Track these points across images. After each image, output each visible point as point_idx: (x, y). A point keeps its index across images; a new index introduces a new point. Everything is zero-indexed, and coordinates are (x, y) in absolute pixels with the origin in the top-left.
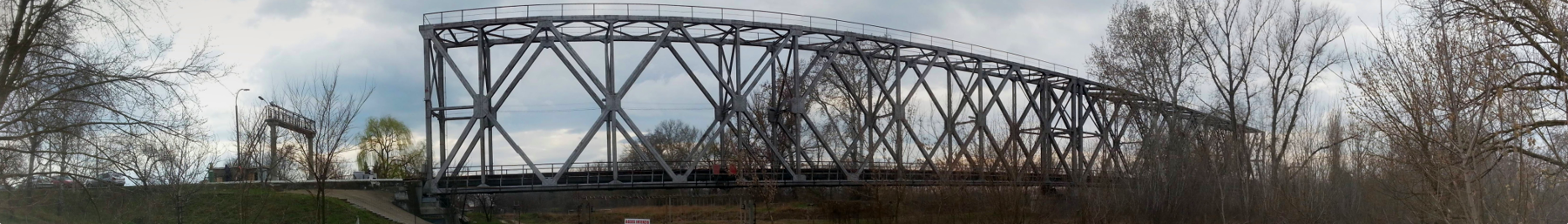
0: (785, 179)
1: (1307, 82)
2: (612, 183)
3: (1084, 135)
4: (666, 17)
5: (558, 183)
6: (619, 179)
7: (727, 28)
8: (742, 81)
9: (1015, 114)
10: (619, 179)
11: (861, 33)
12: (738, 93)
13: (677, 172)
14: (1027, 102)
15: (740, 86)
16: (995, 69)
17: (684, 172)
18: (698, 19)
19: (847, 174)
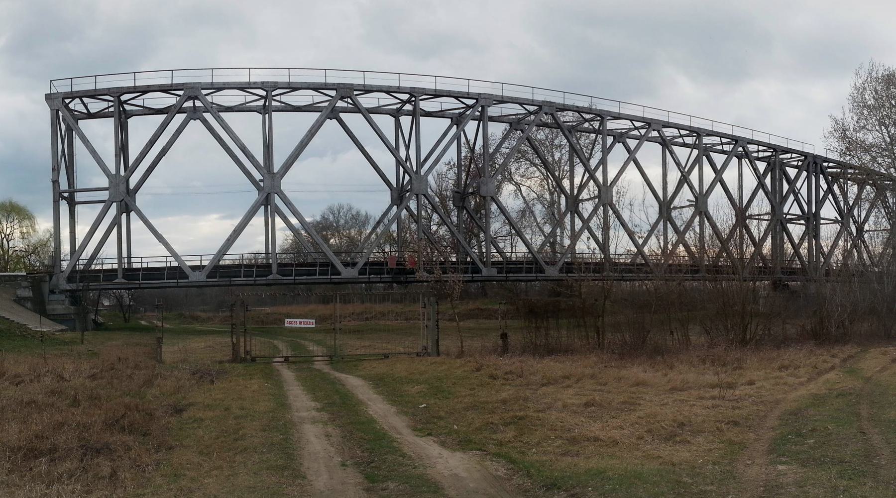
2: (270, 277)
5: (208, 277)
6: (278, 273)
10: (278, 273)
12: (417, 172)
15: (420, 165)
17: (354, 264)
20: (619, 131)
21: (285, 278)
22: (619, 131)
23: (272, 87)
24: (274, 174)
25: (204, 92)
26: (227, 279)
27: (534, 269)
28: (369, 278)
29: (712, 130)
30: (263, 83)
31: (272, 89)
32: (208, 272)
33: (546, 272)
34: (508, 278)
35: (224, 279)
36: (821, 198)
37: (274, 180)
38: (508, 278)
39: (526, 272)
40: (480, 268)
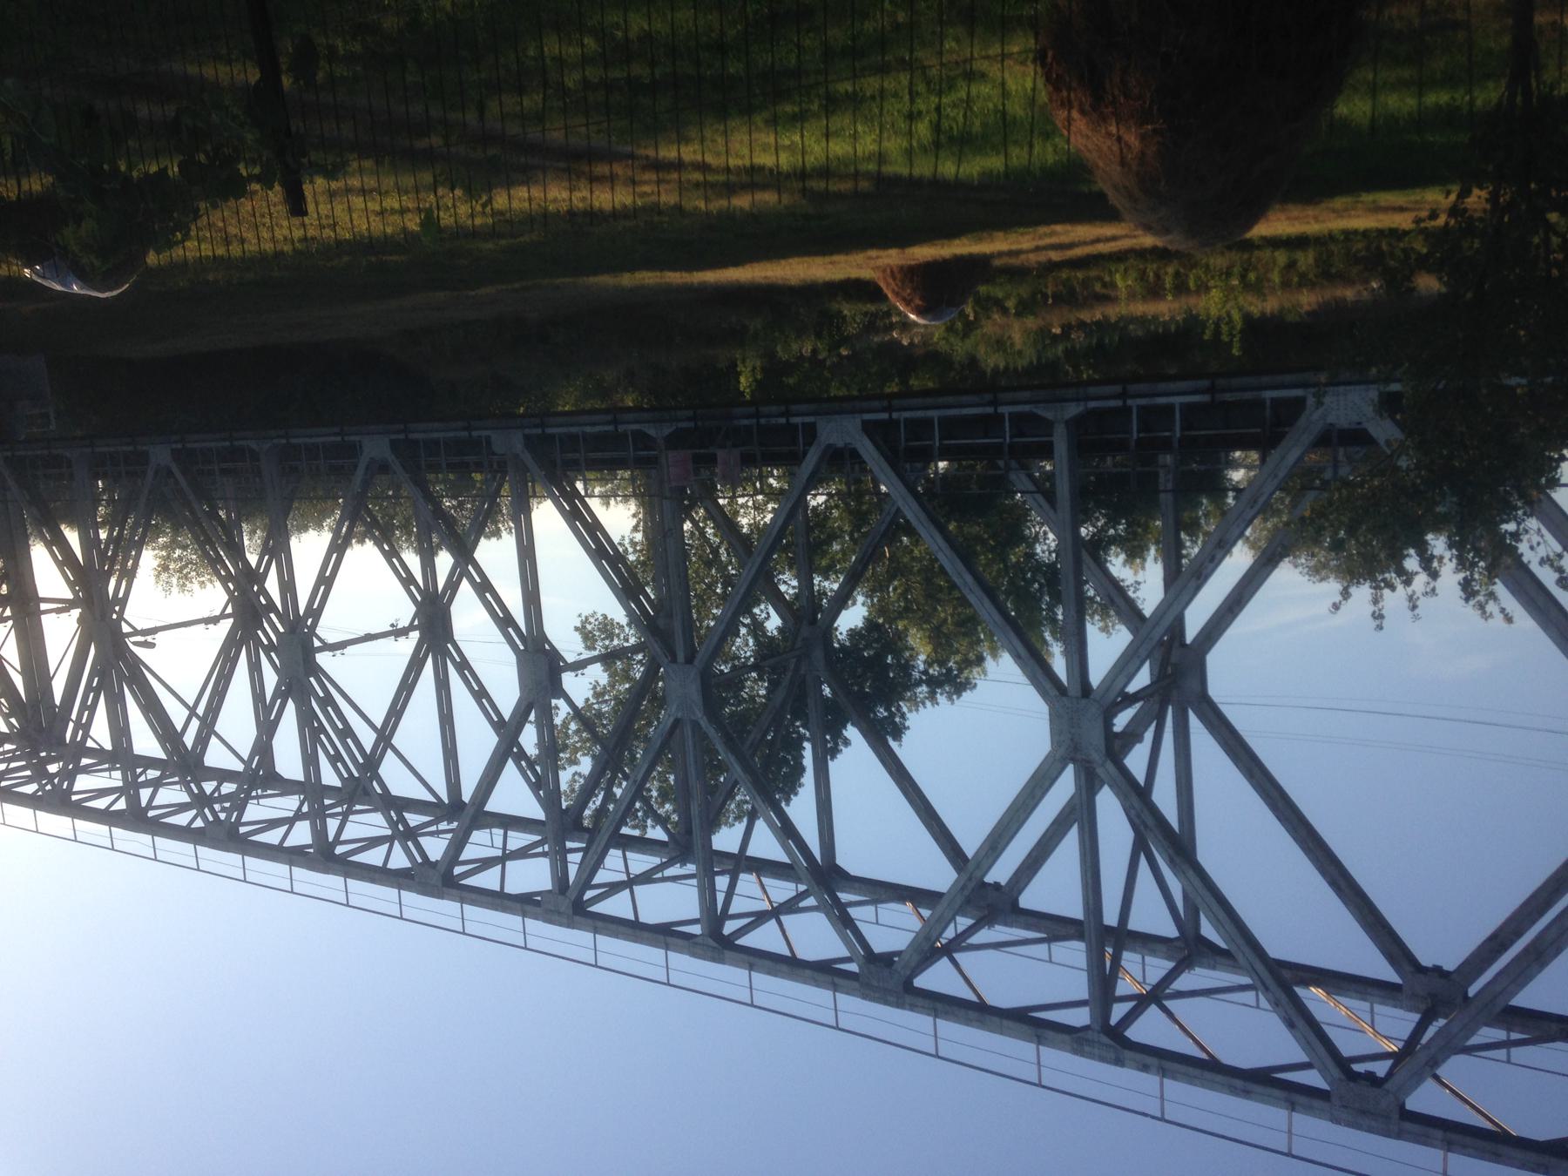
0: (893, 424)
1: (1190, 1049)
2: (1073, 410)
3: (43, 606)
4: (912, 1008)
5: (1300, 403)
6: (1047, 426)
7: (1150, 1029)
8: (1071, 843)
9: (442, 686)
10: (1047, 426)
11: (1298, 1117)
12: (1088, 785)
13: (1356, 437)
14: (491, 740)
15: (1080, 814)
16: (647, 878)
17: (1328, 439)
18: (818, 984)
19: (391, 457)
20: (269, 792)
21: (1027, 408)
22: (269, 792)
23: (1090, 1042)
24: (1073, 760)
25: (853, 967)
26: (1228, 397)
27: (1135, 428)
28: (1123, 395)
29: (577, 866)
30: (1119, 1062)
31: (1089, 1035)
32: (1302, 422)
33: (860, 423)
34: (783, 408)
35: (1237, 396)
36: (448, 660)
37: (1072, 740)
38: (783, 408)
39: (928, 422)
40: (872, 439)
